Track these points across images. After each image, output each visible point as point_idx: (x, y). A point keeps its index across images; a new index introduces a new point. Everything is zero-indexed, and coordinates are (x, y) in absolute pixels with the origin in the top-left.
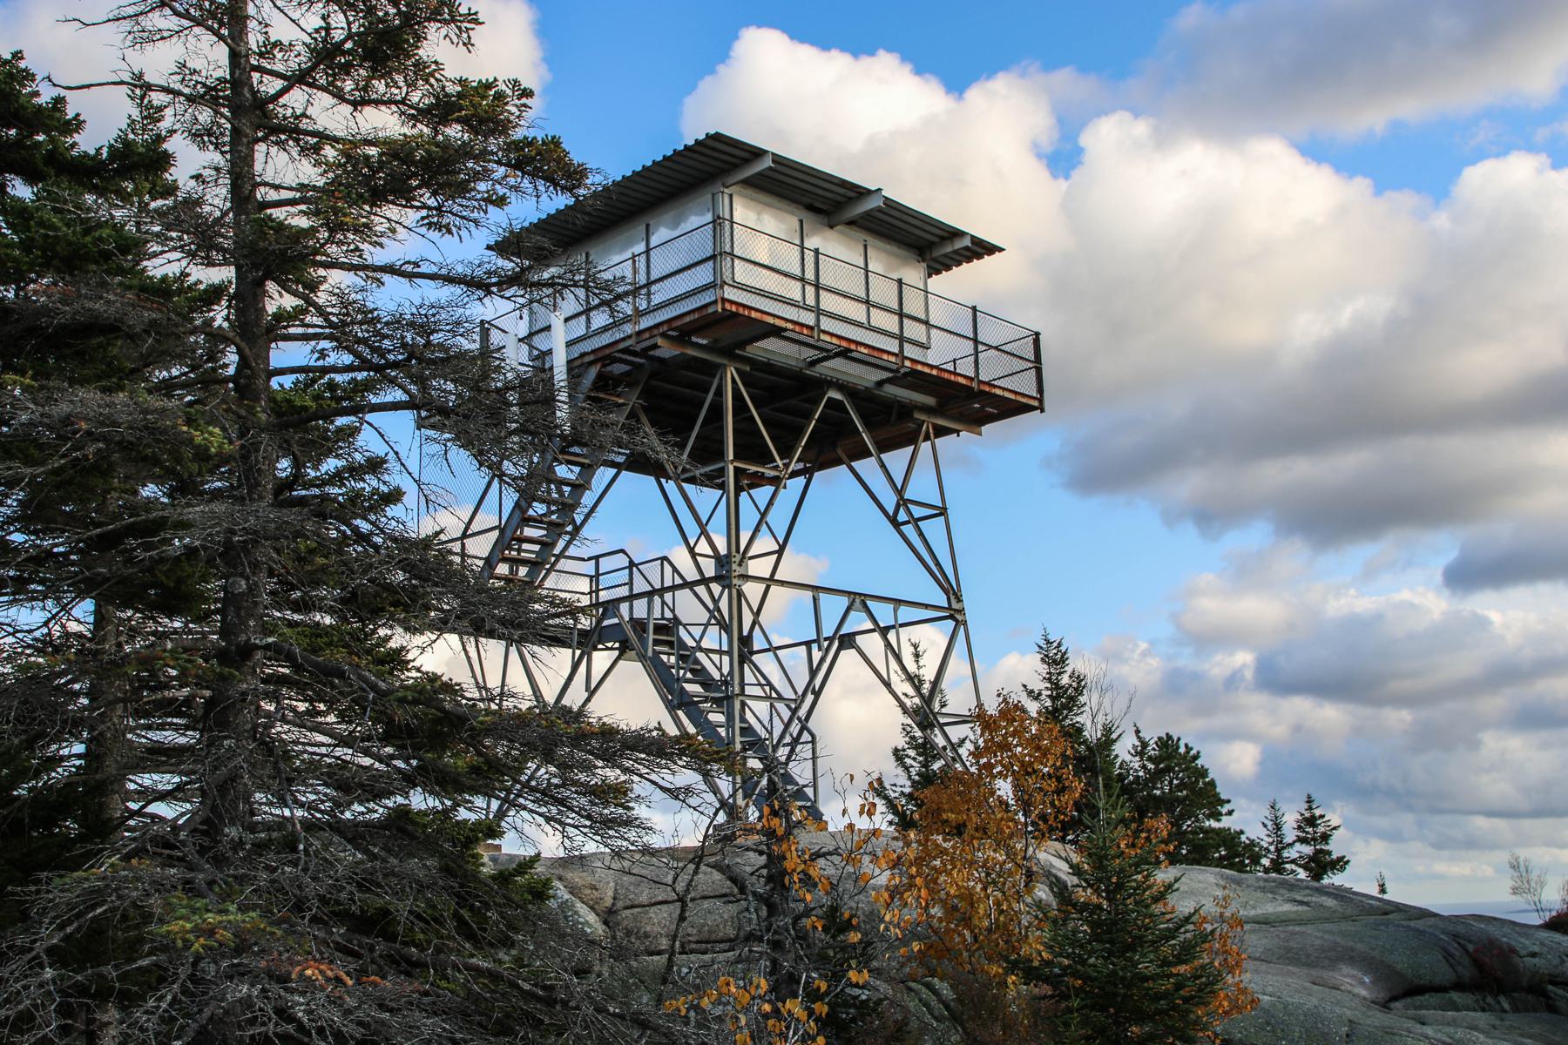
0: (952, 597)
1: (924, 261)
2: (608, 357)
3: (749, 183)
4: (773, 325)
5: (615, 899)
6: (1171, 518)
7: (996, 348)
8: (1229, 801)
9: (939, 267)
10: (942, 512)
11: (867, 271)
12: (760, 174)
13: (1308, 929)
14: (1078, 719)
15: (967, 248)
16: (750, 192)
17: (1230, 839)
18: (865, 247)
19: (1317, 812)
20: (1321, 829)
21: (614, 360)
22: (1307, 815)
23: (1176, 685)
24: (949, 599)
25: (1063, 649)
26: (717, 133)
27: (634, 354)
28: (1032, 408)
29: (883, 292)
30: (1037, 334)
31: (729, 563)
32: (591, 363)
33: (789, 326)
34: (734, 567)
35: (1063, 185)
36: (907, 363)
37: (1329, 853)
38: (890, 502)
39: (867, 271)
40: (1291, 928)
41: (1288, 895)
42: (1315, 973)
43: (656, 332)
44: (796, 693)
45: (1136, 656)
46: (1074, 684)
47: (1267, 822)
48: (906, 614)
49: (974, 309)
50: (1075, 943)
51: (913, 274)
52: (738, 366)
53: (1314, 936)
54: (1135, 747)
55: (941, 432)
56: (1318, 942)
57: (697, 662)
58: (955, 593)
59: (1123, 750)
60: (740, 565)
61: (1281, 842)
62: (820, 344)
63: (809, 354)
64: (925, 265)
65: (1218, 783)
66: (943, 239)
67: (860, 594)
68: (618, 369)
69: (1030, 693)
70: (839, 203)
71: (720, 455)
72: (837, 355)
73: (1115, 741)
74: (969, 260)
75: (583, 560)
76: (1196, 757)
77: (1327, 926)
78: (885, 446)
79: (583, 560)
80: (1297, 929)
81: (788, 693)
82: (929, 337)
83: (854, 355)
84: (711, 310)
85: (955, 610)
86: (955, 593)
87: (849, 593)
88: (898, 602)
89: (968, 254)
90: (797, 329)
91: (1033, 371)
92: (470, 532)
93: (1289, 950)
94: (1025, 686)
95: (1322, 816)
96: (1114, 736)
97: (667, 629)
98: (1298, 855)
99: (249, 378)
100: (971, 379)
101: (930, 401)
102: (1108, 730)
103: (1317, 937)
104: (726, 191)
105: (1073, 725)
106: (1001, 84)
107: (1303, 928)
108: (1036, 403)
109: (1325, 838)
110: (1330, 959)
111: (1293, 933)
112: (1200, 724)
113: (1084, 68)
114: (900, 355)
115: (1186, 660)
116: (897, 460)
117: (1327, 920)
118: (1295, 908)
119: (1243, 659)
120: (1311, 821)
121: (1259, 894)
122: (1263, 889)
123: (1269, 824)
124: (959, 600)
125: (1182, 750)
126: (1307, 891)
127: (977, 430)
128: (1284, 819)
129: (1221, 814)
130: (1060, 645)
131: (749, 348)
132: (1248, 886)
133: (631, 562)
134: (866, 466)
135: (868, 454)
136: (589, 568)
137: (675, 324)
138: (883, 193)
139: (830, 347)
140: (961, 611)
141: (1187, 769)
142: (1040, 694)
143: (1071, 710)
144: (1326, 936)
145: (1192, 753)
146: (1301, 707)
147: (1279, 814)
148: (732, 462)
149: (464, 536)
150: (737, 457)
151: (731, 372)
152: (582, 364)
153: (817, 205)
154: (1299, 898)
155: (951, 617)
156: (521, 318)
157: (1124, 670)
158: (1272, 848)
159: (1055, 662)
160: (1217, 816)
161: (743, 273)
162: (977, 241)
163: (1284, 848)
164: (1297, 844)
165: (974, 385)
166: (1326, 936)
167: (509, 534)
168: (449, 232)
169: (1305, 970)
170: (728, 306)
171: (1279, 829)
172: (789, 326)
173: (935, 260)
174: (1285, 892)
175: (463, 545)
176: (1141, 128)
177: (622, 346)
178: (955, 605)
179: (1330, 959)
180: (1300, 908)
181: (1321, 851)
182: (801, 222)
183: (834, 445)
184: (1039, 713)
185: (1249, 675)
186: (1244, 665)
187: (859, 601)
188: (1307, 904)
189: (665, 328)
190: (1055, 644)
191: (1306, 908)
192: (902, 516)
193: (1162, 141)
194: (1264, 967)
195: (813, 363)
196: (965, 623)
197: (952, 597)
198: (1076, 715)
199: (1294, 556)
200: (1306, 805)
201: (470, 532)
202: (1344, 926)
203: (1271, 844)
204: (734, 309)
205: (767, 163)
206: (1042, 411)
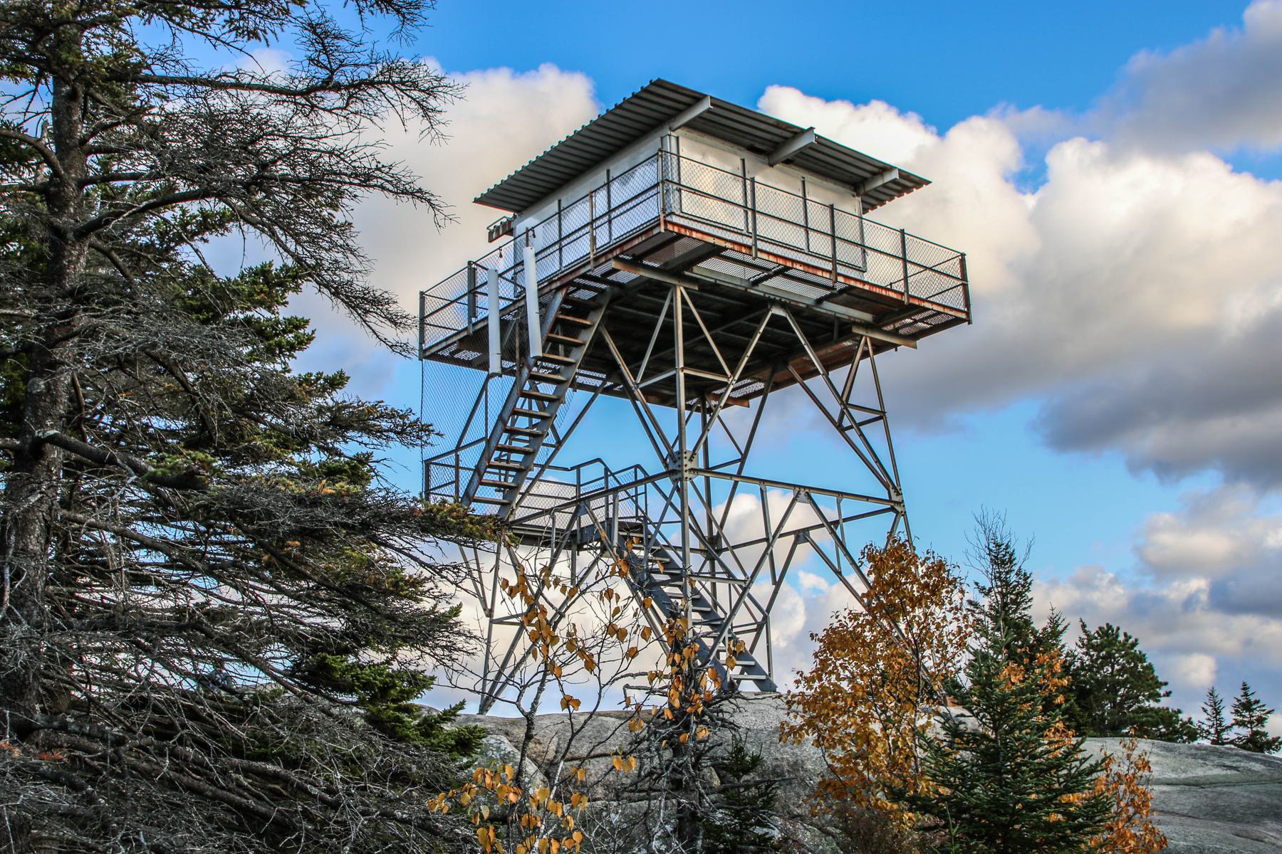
0: (892, 491)
1: (858, 195)
2: (571, 283)
3: (690, 126)
4: (714, 245)
5: (556, 752)
6: (1135, 467)
7: (931, 269)
8: (1166, 684)
9: (873, 202)
10: (881, 415)
11: (805, 200)
12: (699, 117)
13: (1236, 790)
14: (1026, 612)
15: (894, 181)
16: (695, 135)
17: (1168, 718)
18: (803, 182)
19: (1252, 698)
20: (1257, 713)
21: (579, 287)
22: (1243, 700)
23: (1140, 607)
24: (889, 493)
25: (1010, 550)
26: (659, 80)
27: (595, 279)
28: (961, 321)
29: (819, 218)
30: (963, 255)
31: (681, 458)
32: (558, 289)
33: (729, 245)
34: (685, 462)
35: (1030, 201)
36: (841, 279)
37: (1265, 734)
38: (835, 408)
39: (805, 200)
40: (1219, 789)
41: (1217, 761)
42: (1239, 827)
43: (610, 256)
44: (745, 574)
45: (1105, 582)
46: (1022, 582)
47: (1206, 707)
48: (850, 508)
49: (902, 232)
50: (958, 770)
51: (852, 205)
52: (687, 286)
53: (1242, 795)
54: (1081, 640)
55: (880, 347)
56: (1244, 801)
57: (667, 556)
58: (894, 487)
59: (1070, 642)
60: (691, 460)
61: (1220, 725)
62: (757, 262)
63: (752, 274)
64: (859, 199)
65: (1155, 667)
66: (874, 174)
67: (805, 487)
68: (585, 295)
69: (982, 590)
70: (777, 143)
71: (671, 363)
72: (777, 273)
73: (1061, 632)
74: (900, 194)
75: (566, 469)
76: (1134, 645)
77: (1255, 787)
78: (830, 364)
79: (566, 469)
80: (1225, 789)
81: (740, 576)
82: (865, 262)
83: (790, 272)
84: (655, 232)
85: (895, 502)
86: (894, 487)
87: (795, 486)
88: (841, 494)
89: (899, 188)
90: (736, 248)
91: (960, 288)
92: (462, 445)
93: (1216, 807)
94: (977, 584)
95: (1257, 702)
96: (1060, 628)
97: (638, 528)
98: (1236, 736)
99: (57, 185)
100: (902, 294)
101: (867, 317)
102: (1054, 623)
103: (1243, 797)
104: (673, 134)
105: (1021, 618)
106: (977, 123)
107: (1231, 789)
108: (963, 316)
109: (1261, 721)
110: (1256, 815)
111: (1221, 793)
112: (1162, 639)
113: (1049, 106)
114: (834, 273)
115: (1148, 587)
116: (839, 376)
117: (1255, 782)
118: (1224, 772)
119: (1198, 584)
120: (1248, 706)
121: (1190, 760)
122: (1194, 756)
123: (1209, 709)
124: (899, 494)
125: (1121, 638)
126: (1237, 758)
127: (913, 343)
128: (1222, 705)
129: (1159, 695)
130: (1007, 547)
131: (695, 269)
132: (1180, 754)
133: (607, 469)
134: (816, 383)
135: (816, 373)
136: (571, 477)
137: (626, 248)
138: (815, 132)
139: (770, 266)
140: (900, 503)
141: (1126, 654)
142: (990, 590)
143: (1018, 604)
144: (1252, 796)
145: (1130, 641)
146: (1248, 624)
147: (1218, 700)
148: (682, 370)
149: (458, 448)
150: (687, 365)
151: (680, 291)
152: (551, 290)
153: (757, 146)
154: (1228, 763)
155: (892, 509)
156: (501, 256)
157: (1095, 596)
158: (1212, 731)
159: (1003, 562)
160: (1155, 697)
161: (690, 204)
162: (904, 175)
163: (1223, 730)
164: (1235, 727)
165: (905, 299)
166: (1252, 796)
167: (493, 444)
168: (257, 37)
169: (1231, 824)
170: (670, 227)
171: (1218, 713)
172: (729, 245)
173: (866, 194)
174: (1216, 758)
175: (457, 457)
176: (1097, 149)
177: (583, 271)
178: (895, 498)
179: (1256, 815)
180: (1229, 772)
181: (1257, 733)
182: (743, 161)
183: (786, 364)
184: (991, 607)
185: (1204, 597)
186: (1199, 591)
187: (804, 493)
188: (1236, 768)
189: (618, 251)
190: (1003, 547)
191: (1234, 772)
192: (846, 423)
193: (1115, 158)
194: (1189, 821)
195: (756, 283)
196: (904, 514)
197: (892, 491)
198: (1024, 609)
199: (1242, 498)
200: (1242, 693)
201: (462, 445)
202: (1270, 787)
203: (1212, 727)
204: (676, 230)
205: (706, 105)
206: (970, 323)
